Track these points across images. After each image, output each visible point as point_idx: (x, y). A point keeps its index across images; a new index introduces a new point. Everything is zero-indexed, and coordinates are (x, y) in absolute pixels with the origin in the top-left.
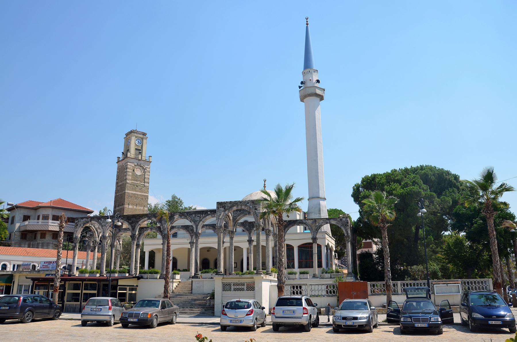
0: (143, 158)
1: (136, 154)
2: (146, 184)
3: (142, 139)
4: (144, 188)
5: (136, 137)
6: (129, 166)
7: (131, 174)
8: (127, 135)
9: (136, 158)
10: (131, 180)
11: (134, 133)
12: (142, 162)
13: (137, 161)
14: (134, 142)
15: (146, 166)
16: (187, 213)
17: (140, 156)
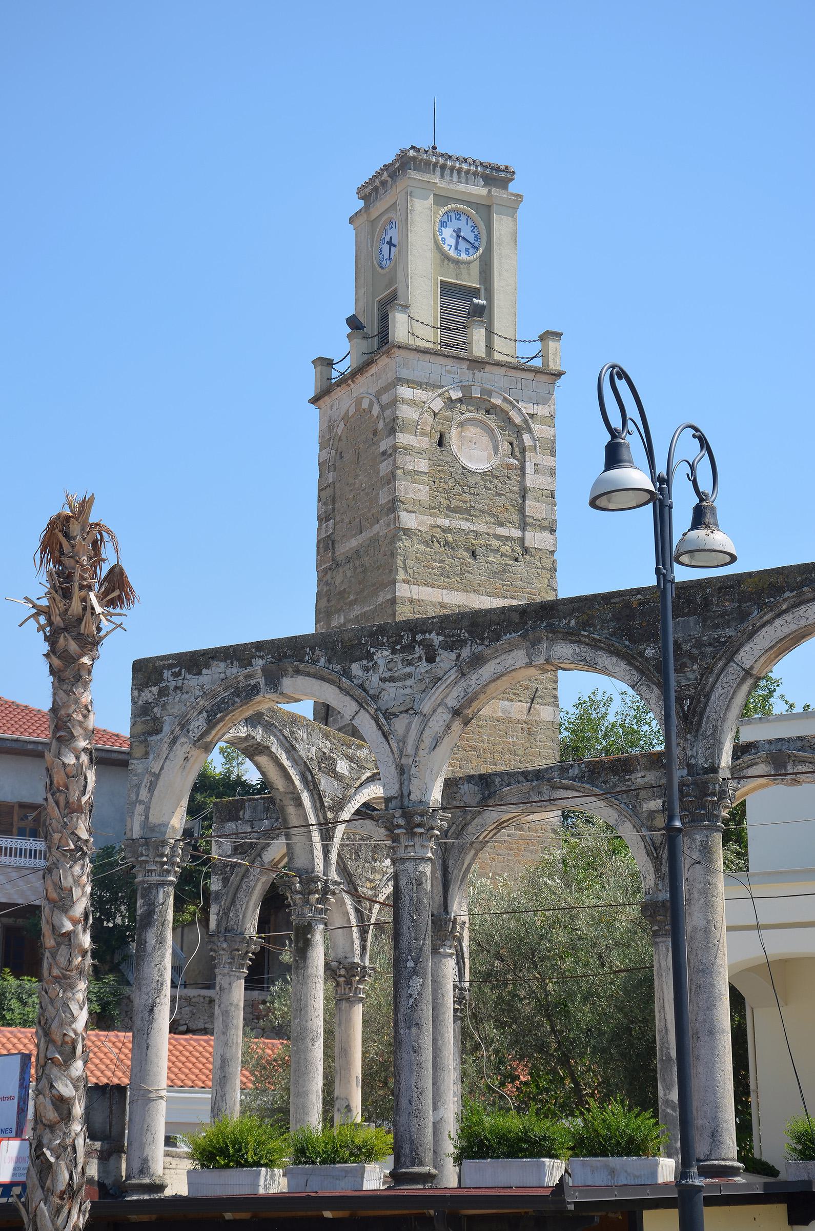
0: (503, 350)
2: (535, 539)
3: (485, 210)
4: (520, 568)
5: (441, 199)
6: (406, 412)
7: (423, 465)
8: (370, 192)
10: (431, 509)
11: (427, 166)
12: (493, 378)
13: (463, 372)
15: (527, 408)
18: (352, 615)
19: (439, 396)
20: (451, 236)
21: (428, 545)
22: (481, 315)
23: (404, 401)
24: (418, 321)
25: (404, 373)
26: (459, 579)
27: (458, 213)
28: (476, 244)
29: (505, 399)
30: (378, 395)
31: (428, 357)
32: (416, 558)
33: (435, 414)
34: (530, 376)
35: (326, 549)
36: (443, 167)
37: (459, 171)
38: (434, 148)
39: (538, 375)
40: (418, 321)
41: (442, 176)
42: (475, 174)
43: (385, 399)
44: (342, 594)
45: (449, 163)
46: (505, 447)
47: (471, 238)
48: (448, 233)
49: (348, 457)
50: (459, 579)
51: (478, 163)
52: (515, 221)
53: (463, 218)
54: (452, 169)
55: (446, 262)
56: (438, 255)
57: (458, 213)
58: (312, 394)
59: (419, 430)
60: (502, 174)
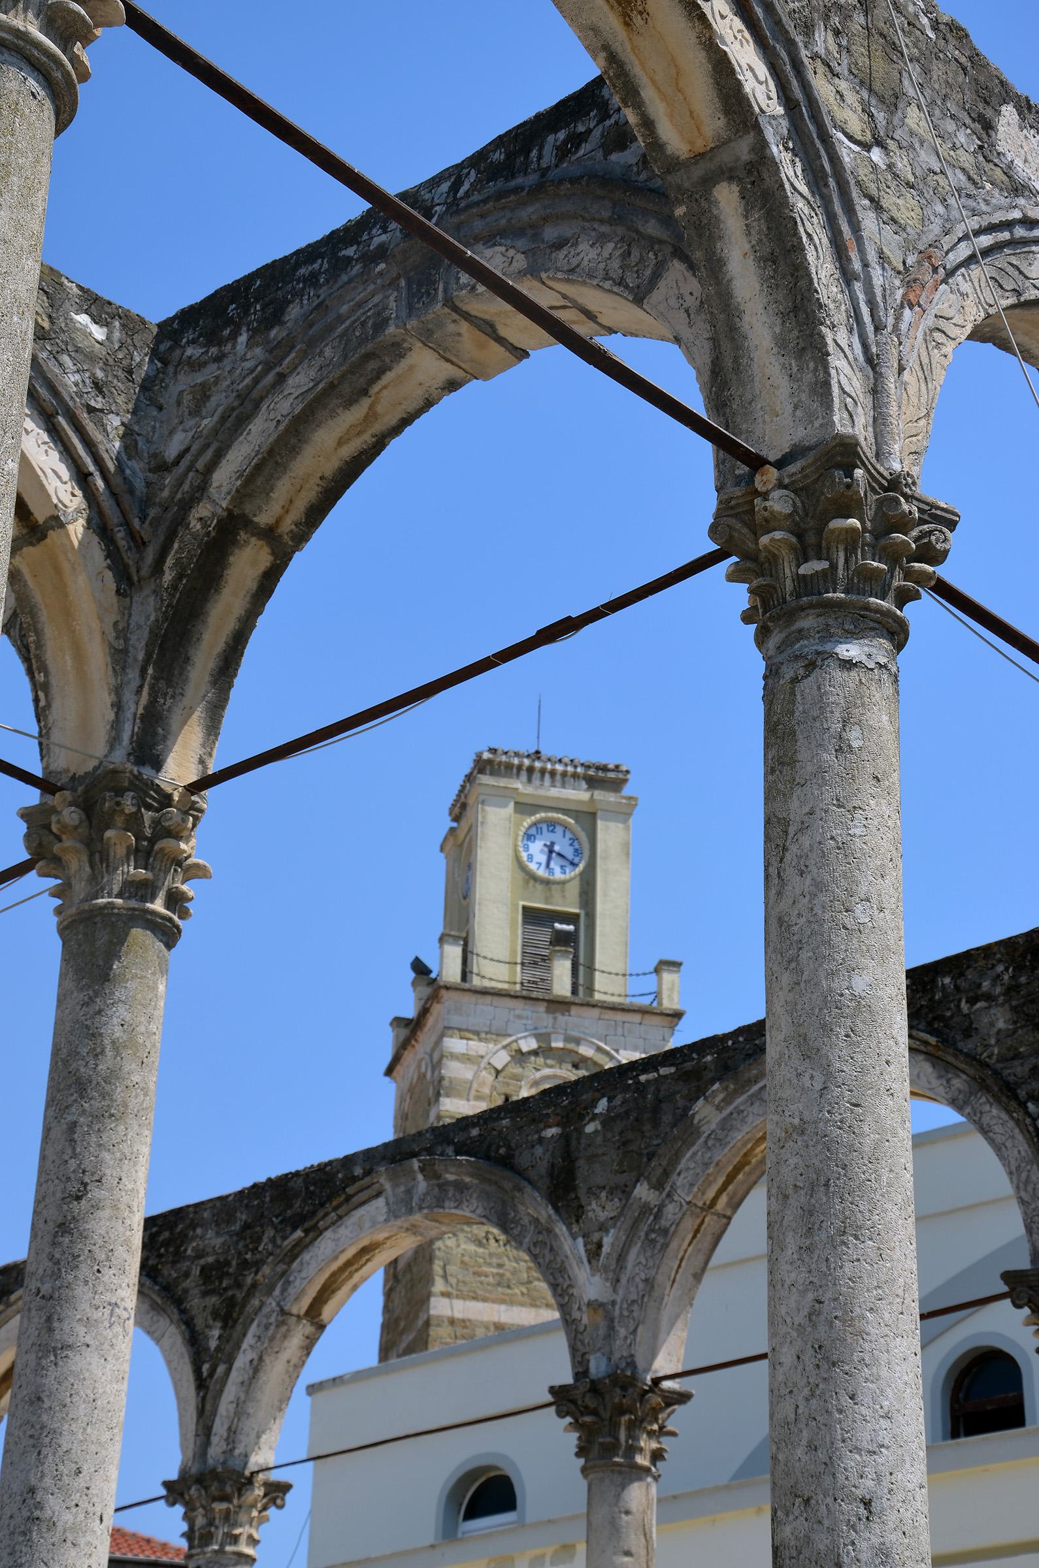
1: (535, 960)
3: (588, 818)
5: (524, 808)
6: (454, 1070)
9: (533, 995)
13: (540, 1015)
14: (504, 845)
16: (94, 495)
17: (562, 969)
19: (504, 1047)
20: (542, 851)
21: (480, 1244)
22: (566, 944)
23: (454, 1056)
24: (485, 958)
25: (456, 1020)
26: (525, 1290)
27: (552, 824)
28: (576, 860)
29: (599, 1049)
31: (488, 999)
32: (462, 1262)
33: (498, 1072)
34: (637, 1018)
36: (530, 770)
37: (553, 773)
38: (538, 752)
39: (647, 1016)
40: (485, 958)
41: (530, 780)
42: (575, 776)
45: (538, 764)
47: (569, 853)
48: (537, 848)
50: (525, 1290)
51: (553, 759)
52: (627, 829)
53: (559, 830)
54: (543, 771)
55: (532, 882)
56: (520, 876)
57: (552, 824)
59: (473, 1093)
60: (612, 775)
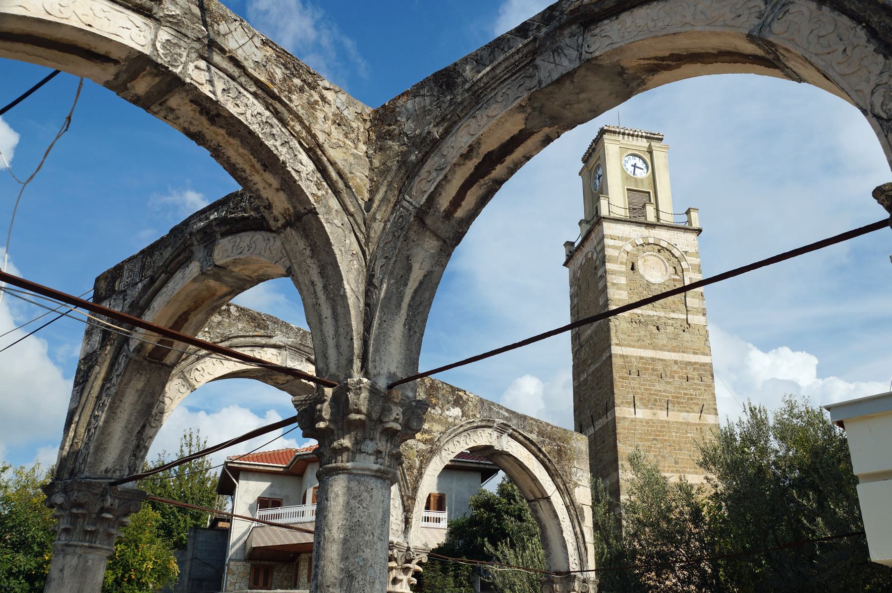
4: (686, 336)
7: (623, 281)
18: (590, 372)
23: (609, 246)
30: (595, 249)
35: (576, 340)
43: (598, 249)
44: (585, 361)
46: (672, 270)
49: (583, 287)
58: (564, 260)
